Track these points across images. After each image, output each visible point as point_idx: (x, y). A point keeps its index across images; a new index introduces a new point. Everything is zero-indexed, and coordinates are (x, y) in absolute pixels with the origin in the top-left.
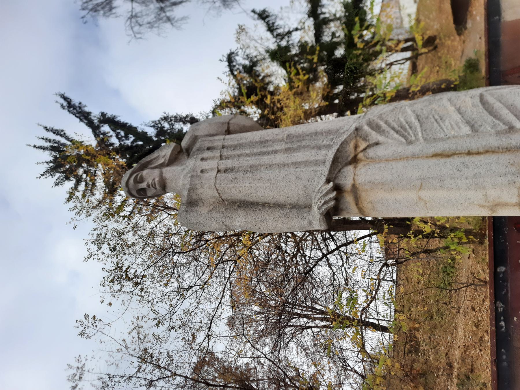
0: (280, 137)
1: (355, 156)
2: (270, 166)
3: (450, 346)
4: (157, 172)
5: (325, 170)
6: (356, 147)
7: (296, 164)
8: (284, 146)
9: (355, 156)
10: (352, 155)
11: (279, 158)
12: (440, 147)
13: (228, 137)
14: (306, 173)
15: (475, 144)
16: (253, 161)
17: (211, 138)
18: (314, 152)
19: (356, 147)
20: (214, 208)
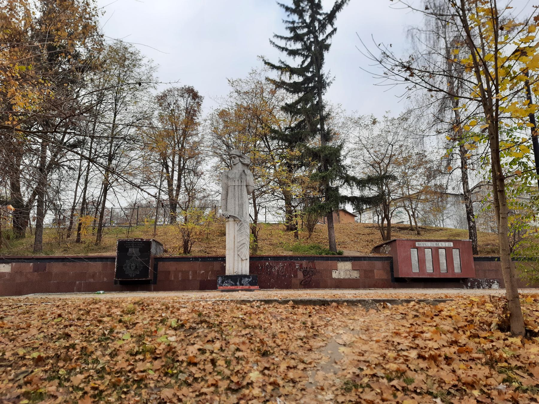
3: (218, 248)
4: (239, 161)
5: (233, 214)
7: (235, 207)
11: (237, 203)
12: (236, 237)
14: (233, 210)
15: (236, 242)
16: (237, 195)
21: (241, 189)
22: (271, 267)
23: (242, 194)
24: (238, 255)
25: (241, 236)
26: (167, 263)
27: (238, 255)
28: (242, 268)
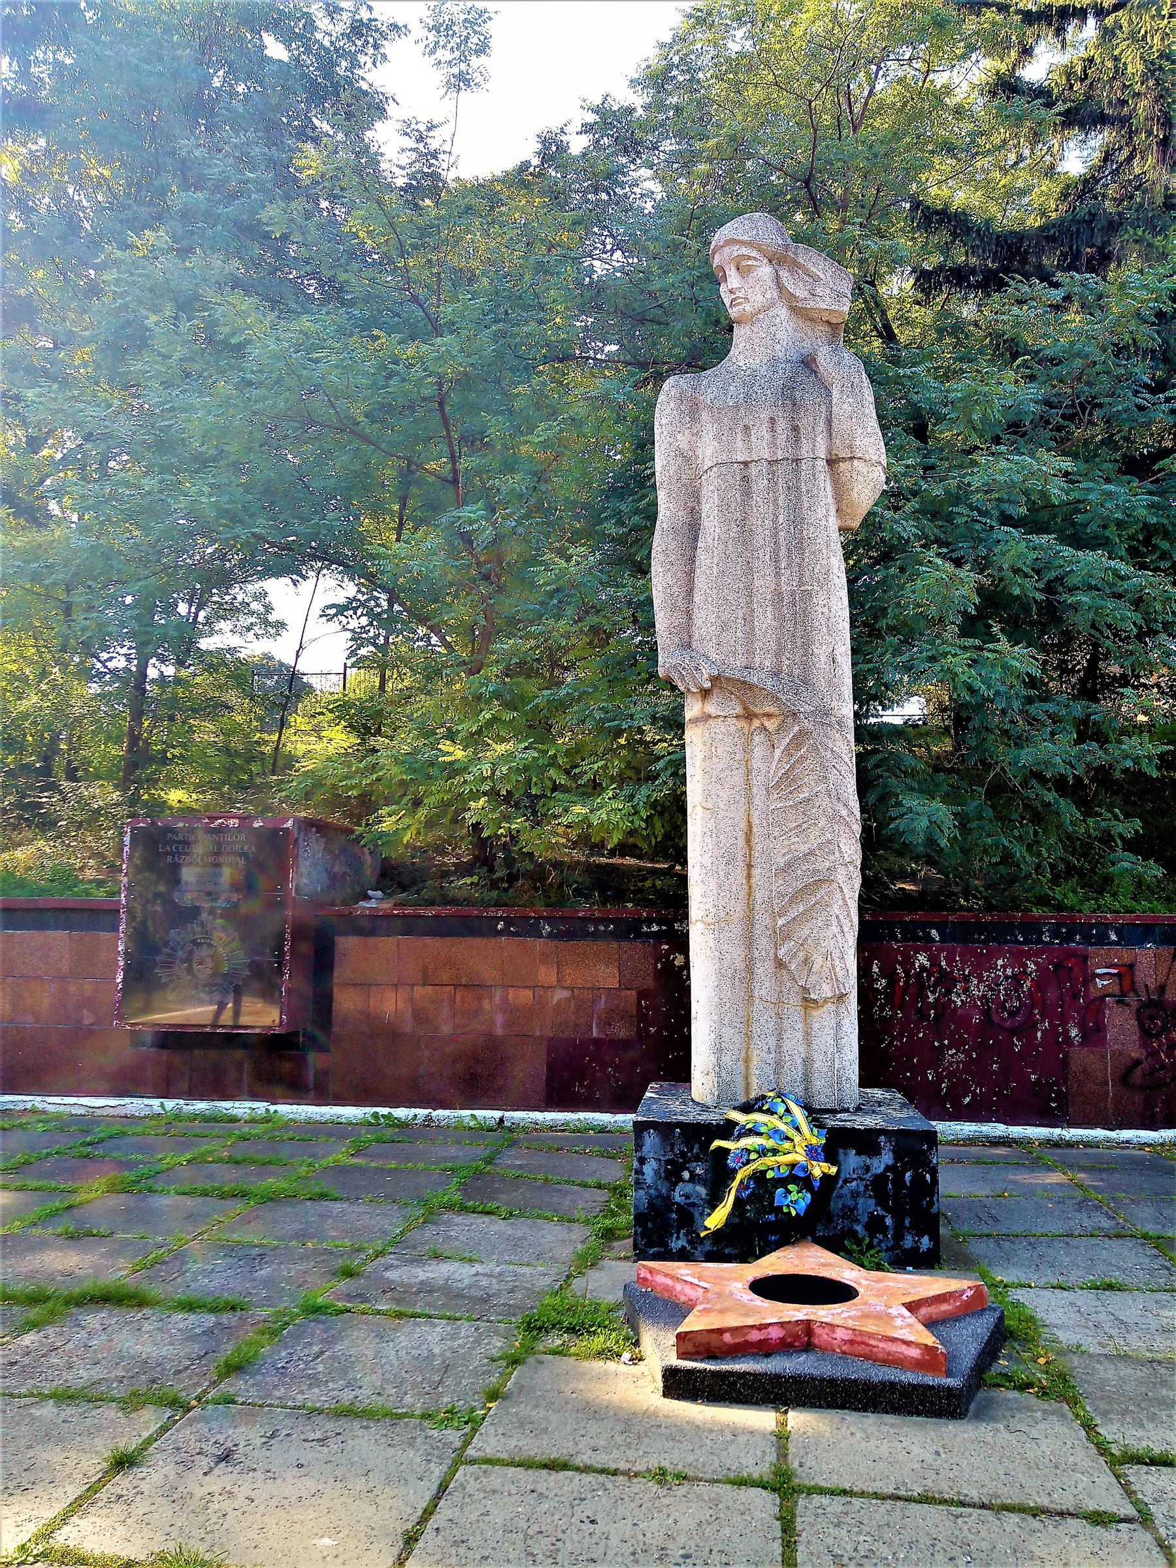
0: (807, 578)
1: (756, 716)
2: (749, 569)
4: (773, 294)
6: (769, 716)
7: (749, 619)
8: (784, 588)
9: (756, 716)
10: (757, 710)
11: (763, 583)
13: (821, 464)
16: (762, 535)
17: (821, 426)
18: (773, 646)
19: (769, 716)
20: (687, 460)
21: (793, 489)
22: (947, 981)
23: (797, 520)
24: (780, 964)
25: (801, 830)
26: (59, 1508)
27: (780, 964)
28: (807, 1062)
